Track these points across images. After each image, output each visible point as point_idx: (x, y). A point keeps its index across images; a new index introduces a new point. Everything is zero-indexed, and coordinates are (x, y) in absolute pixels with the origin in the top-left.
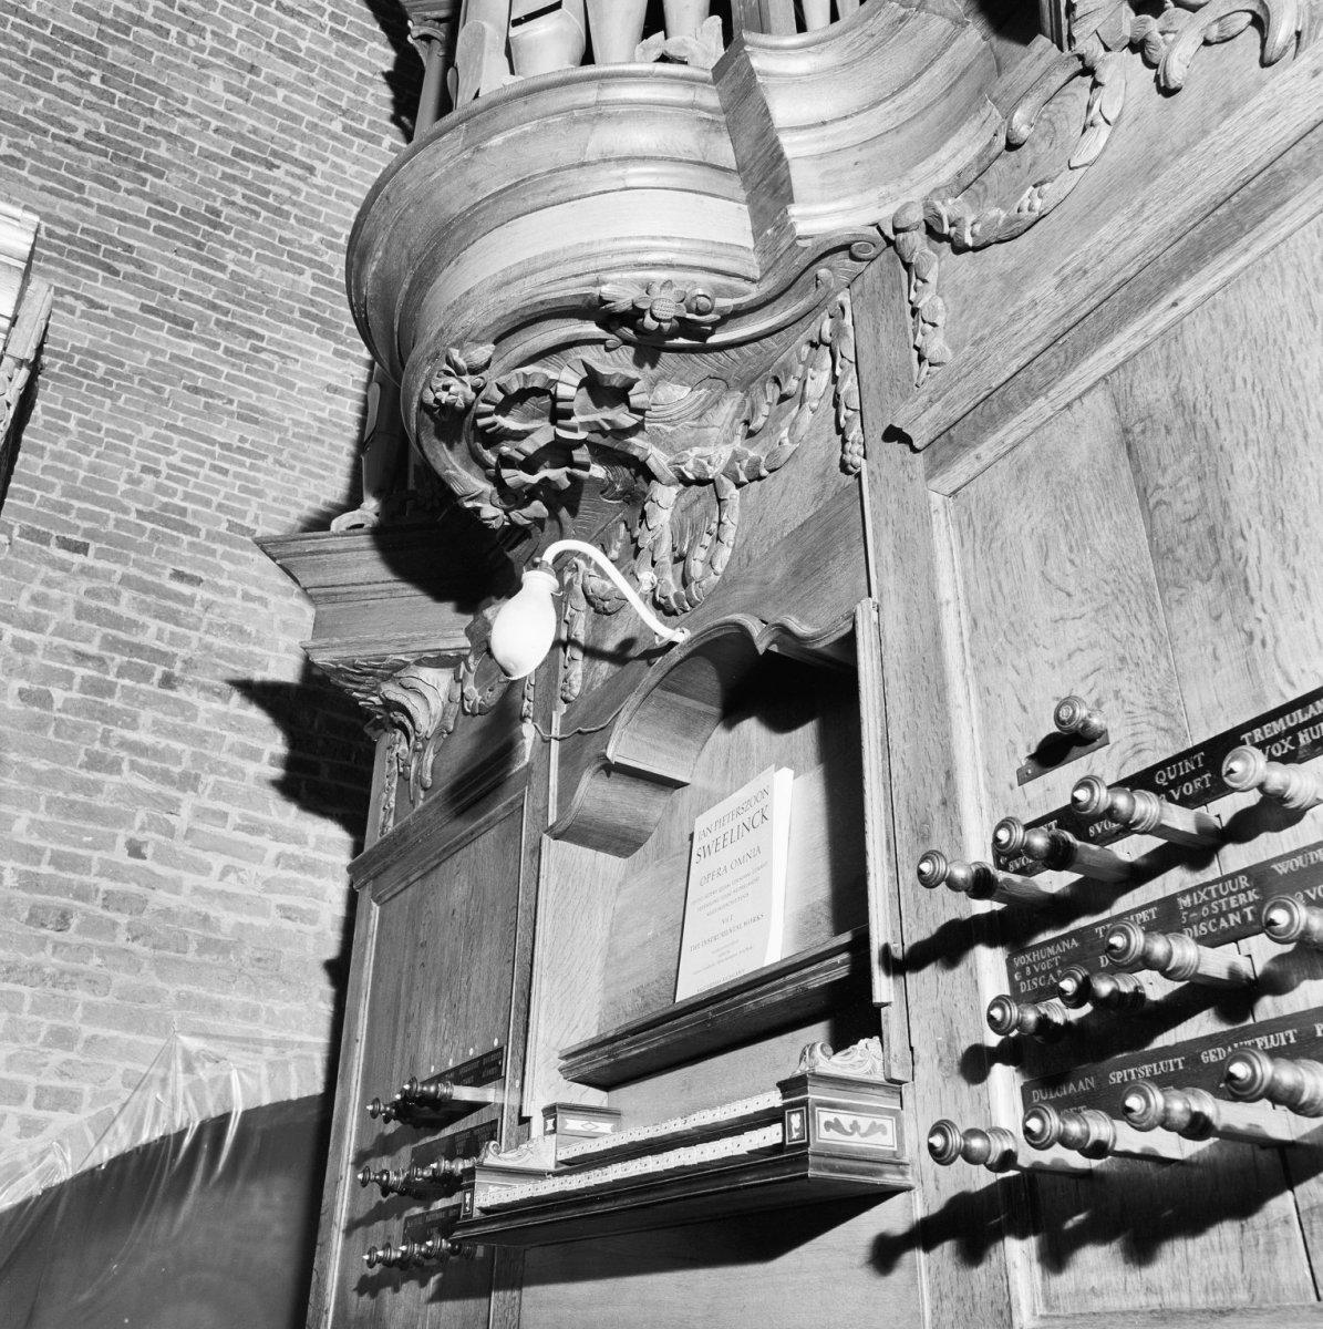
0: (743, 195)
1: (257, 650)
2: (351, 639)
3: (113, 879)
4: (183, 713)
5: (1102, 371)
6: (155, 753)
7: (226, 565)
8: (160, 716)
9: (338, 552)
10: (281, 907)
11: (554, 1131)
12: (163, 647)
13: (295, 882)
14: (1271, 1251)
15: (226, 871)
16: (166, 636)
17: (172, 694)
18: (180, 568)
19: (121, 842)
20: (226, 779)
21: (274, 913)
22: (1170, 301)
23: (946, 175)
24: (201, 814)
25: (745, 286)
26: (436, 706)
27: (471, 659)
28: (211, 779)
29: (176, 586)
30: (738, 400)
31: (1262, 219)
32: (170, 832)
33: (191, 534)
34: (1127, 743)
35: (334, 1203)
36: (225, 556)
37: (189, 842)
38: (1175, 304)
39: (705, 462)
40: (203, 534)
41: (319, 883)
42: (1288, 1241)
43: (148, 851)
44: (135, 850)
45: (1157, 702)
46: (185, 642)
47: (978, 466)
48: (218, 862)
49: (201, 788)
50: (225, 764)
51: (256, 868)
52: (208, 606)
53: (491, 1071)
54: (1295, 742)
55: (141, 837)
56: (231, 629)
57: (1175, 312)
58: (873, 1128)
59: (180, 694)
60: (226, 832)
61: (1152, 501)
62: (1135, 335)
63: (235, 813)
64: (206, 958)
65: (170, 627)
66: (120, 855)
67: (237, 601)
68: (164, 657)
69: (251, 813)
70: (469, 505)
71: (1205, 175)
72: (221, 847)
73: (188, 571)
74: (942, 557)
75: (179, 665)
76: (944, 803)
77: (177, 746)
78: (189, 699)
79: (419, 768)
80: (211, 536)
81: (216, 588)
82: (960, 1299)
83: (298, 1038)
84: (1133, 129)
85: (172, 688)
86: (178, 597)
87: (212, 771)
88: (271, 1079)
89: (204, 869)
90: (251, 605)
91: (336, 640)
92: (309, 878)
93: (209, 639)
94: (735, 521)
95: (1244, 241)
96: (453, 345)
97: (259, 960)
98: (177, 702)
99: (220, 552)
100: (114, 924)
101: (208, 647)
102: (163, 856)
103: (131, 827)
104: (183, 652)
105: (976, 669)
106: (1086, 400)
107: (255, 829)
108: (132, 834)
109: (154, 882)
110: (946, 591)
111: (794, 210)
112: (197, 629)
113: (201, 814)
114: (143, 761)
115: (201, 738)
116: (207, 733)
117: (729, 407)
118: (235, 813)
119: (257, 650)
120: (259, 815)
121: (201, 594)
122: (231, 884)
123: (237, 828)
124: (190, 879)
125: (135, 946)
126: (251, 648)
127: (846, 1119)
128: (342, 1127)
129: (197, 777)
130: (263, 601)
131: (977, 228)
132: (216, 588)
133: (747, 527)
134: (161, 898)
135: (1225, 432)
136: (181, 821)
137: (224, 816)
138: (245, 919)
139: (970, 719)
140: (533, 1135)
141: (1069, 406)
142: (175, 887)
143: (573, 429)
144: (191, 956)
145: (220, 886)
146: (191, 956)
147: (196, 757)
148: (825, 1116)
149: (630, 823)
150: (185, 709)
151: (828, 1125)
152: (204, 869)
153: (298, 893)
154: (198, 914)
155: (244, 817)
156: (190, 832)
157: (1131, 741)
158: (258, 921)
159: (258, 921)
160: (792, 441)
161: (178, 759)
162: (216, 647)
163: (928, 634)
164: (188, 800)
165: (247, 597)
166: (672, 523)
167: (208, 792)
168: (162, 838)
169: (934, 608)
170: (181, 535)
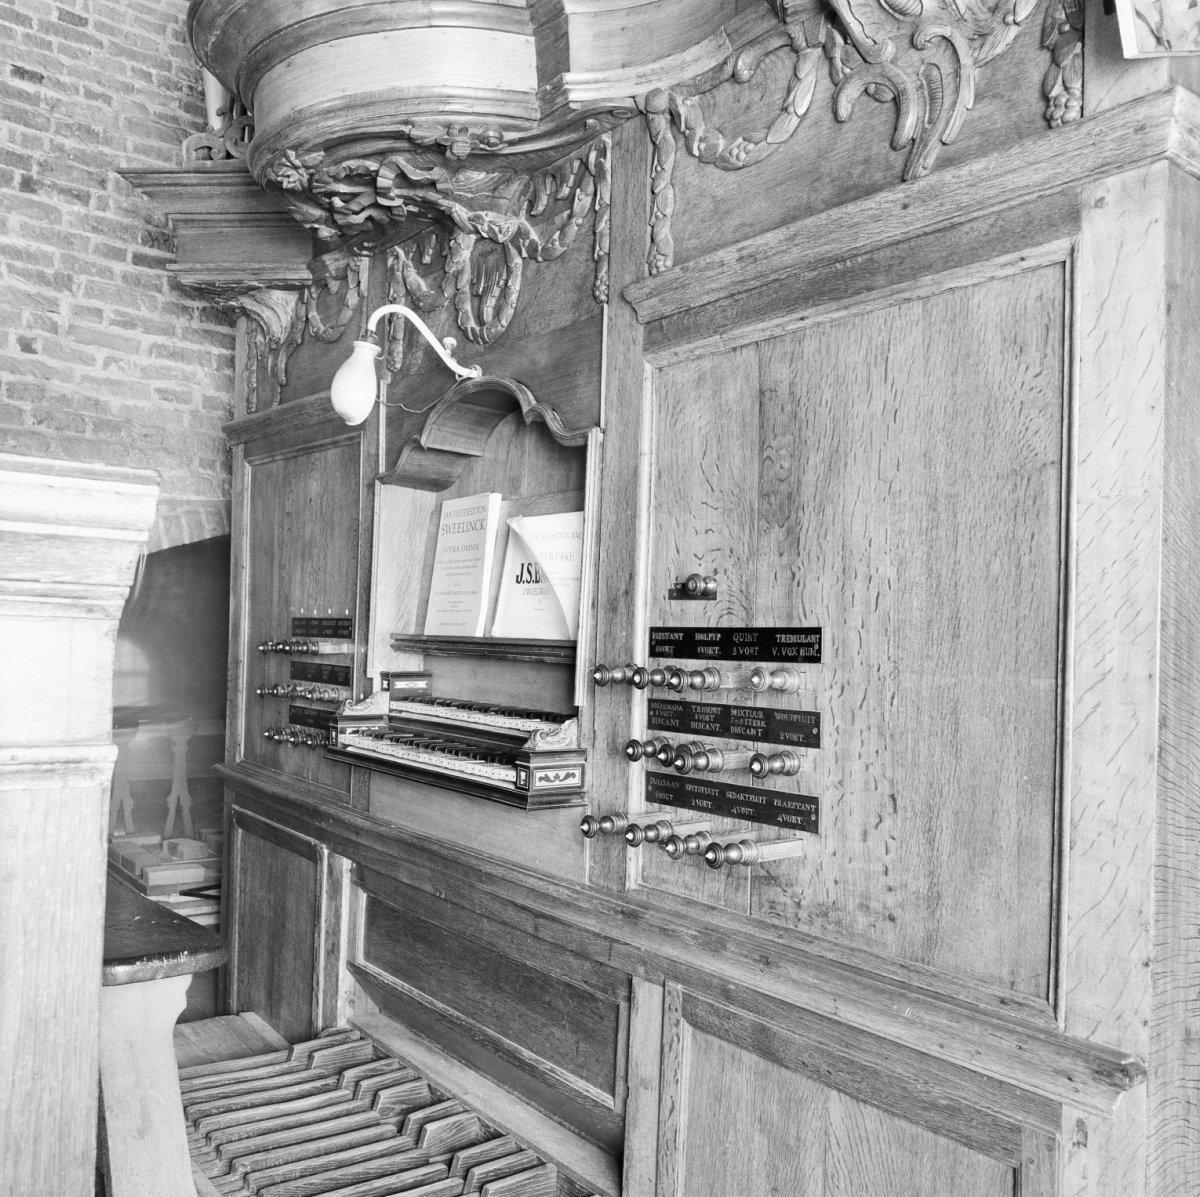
0: (531, 27)
1: (107, 150)
2: (211, 266)
3: (13, 372)
4: (47, 216)
5: (756, 337)
6: (30, 256)
7: (64, 59)
8: (27, 220)
9: (192, 185)
10: (159, 391)
11: (387, 690)
12: (18, 149)
13: (169, 369)
14: (737, 889)
15: (107, 364)
16: (19, 138)
17: (34, 197)
18: (20, 64)
19: (13, 339)
20: (97, 279)
21: (155, 396)
22: (800, 315)
23: (688, 75)
24: (78, 311)
25: (527, 124)
26: (286, 320)
27: (313, 290)
28: (83, 278)
29: (18, 83)
30: (524, 182)
31: (858, 292)
32: (54, 328)
33: (23, 25)
34: (725, 605)
35: (237, 677)
36: (63, 50)
37: (72, 337)
38: (802, 319)
39: (496, 229)
40: (35, 23)
41: (189, 368)
42: (745, 887)
43: (38, 346)
44: (27, 346)
45: (744, 588)
46: (35, 143)
47: (674, 359)
48: (101, 354)
49: (74, 288)
50: (94, 265)
51: (134, 358)
52: (54, 105)
53: (345, 632)
54: (798, 652)
55: (29, 334)
56: (79, 129)
57: (801, 324)
58: (567, 776)
59: (41, 197)
60: (103, 327)
61: (766, 454)
62: (778, 326)
63: (109, 309)
64: (102, 436)
65: (21, 128)
66: (14, 350)
67: (80, 99)
68: (22, 161)
69: (123, 309)
70: (308, 226)
71: (833, 236)
72: (100, 340)
73: (28, 67)
74: (646, 418)
75: (35, 168)
76: (627, 593)
77: (49, 249)
78: (51, 203)
79: (275, 365)
80: (46, 27)
81: (58, 85)
82: (603, 866)
83: (185, 498)
84: (812, 132)
85: (33, 191)
86: (21, 95)
87: (83, 271)
88: (168, 530)
89: (89, 361)
90: (94, 103)
91: (198, 266)
92: (180, 365)
93: (60, 139)
94: (518, 288)
95: (846, 302)
96: (290, 148)
97: (146, 435)
98: (40, 205)
99: (55, 46)
100: (21, 411)
101: (61, 149)
102: (52, 350)
103: (20, 325)
104: (37, 155)
105: (656, 508)
106: (744, 351)
107: (128, 324)
108: (21, 332)
109: (48, 373)
110: (646, 445)
111: (568, 77)
112: (47, 130)
113: (78, 311)
114: (19, 264)
115: (67, 240)
116: (74, 236)
117: (516, 187)
118: (109, 309)
119: (107, 150)
120: (130, 310)
121: (46, 91)
122: (113, 373)
123: (113, 323)
124: (80, 370)
125: (42, 428)
126: (101, 148)
127: (551, 774)
128: (237, 627)
129: (70, 278)
130: (108, 100)
131: (703, 146)
132: (58, 85)
133: (526, 297)
134: (56, 386)
135: (810, 433)
136: (63, 317)
137: (99, 312)
138: (130, 402)
139: (648, 543)
140: (374, 691)
141: (735, 349)
142: (67, 377)
143: (392, 199)
144: (88, 435)
145: (104, 374)
146: (88, 435)
147: (66, 259)
148: (539, 774)
149: (438, 477)
150: (49, 212)
151: (541, 779)
152: (89, 361)
153: (170, 377)
154: (89, 399)
155: (118, 313)
156: (72, 328)
157: (728, 604)
158: (141, 403)
159: (141, 403)
160: (561, 245)
161: (48, 260)
162: (67, 148)
163: (631, 472)
164: (65, 300)
165: (89, 94)
166: (471, 259)
167: (82, 290)
168: (48, 334)
169: (637, 456)
170: (13, 26)
